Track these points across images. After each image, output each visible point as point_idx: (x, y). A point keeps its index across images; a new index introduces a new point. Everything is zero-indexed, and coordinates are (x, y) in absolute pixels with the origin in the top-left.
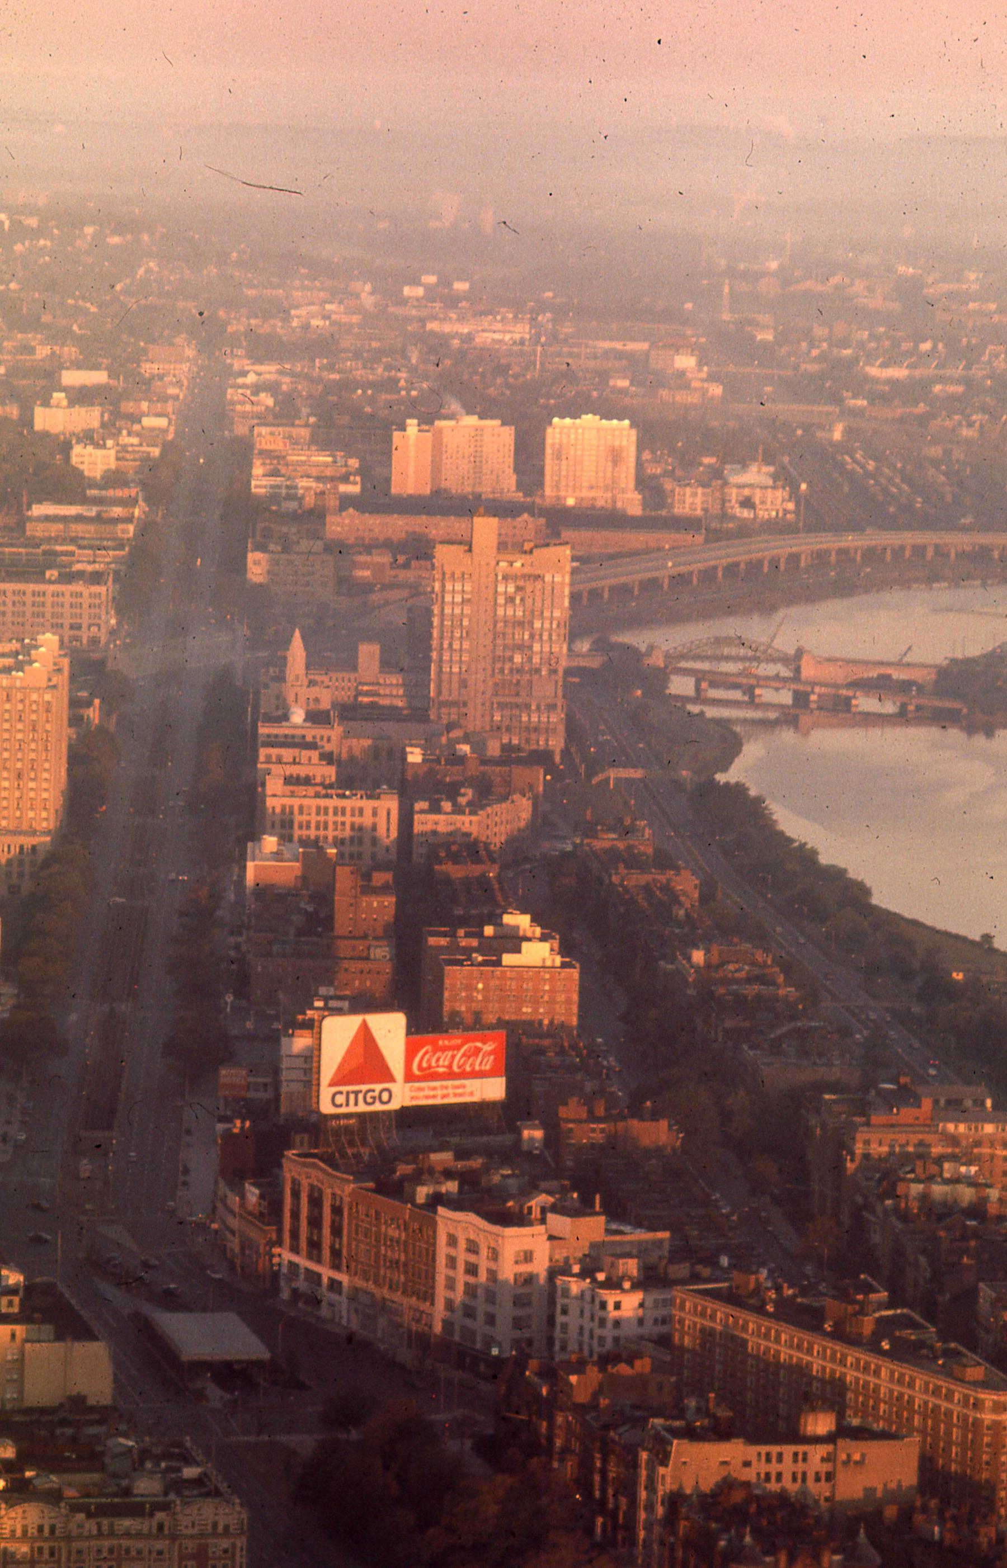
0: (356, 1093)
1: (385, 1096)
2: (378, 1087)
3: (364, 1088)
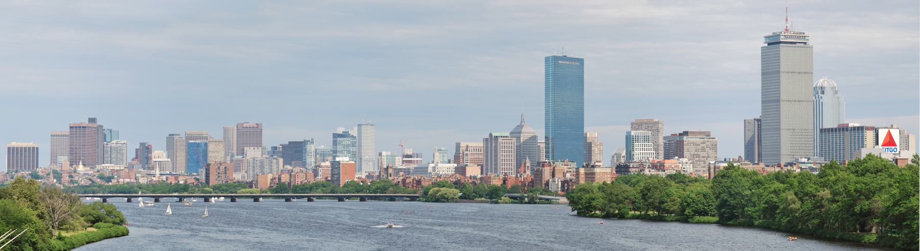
0: (888, 149)
1: (895, 150)
2: (893, 147)
3: (890, 147)
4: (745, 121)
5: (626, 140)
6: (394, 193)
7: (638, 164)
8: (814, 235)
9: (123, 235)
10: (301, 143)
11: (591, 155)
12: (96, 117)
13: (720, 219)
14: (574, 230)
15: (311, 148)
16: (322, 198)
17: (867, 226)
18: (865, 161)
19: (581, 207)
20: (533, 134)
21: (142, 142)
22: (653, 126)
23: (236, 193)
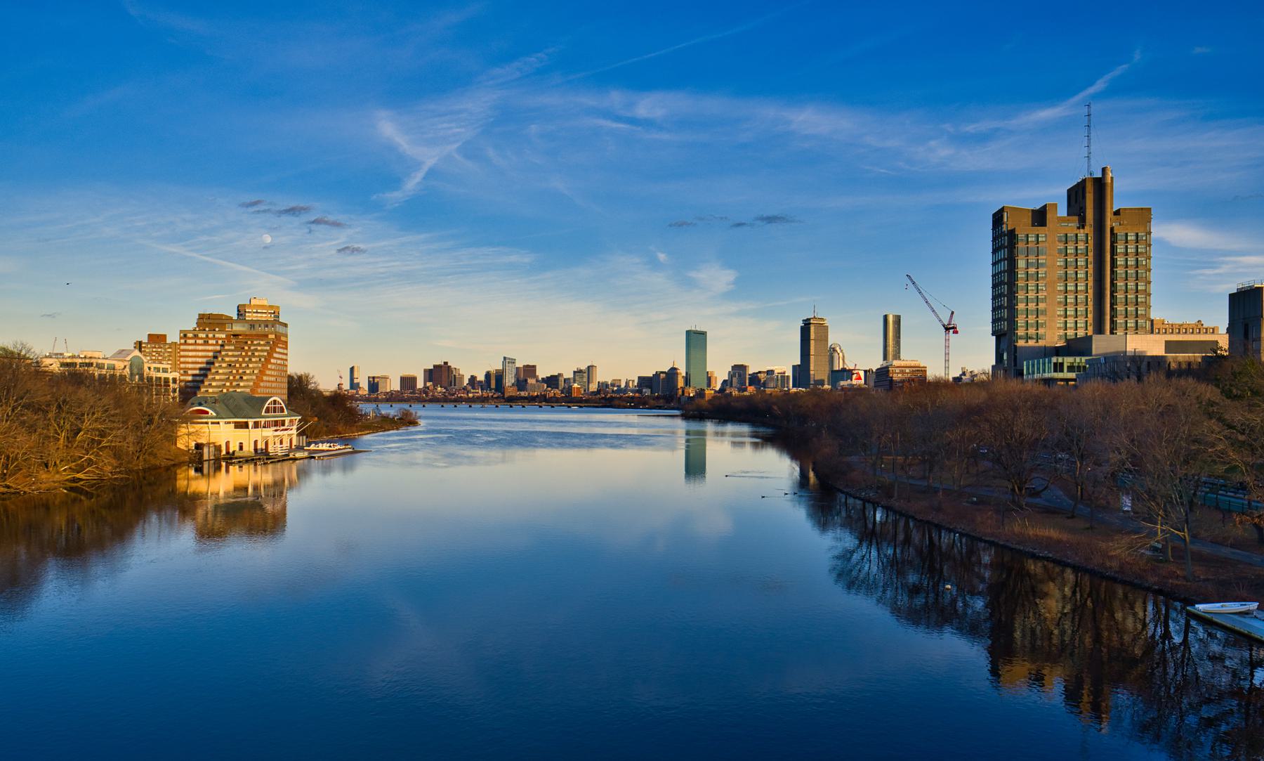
4: (505, 358)
5: (686, 354)
6: (304, 430)
7: (900, 591)
8: (7, 469)
9: (900, 320)
10: (556, 376)
11: (288, 388)
12: (415, 375)
13: (929, 382)
14: (502, 439)
15: (561, 379)
16: (567, 440)
17: (179, 515)
18: (599, 392)
19: (1193, 492)
20: (368, 457)
21: (1103, 335)
22: (513, 361)
23: (235, 422)
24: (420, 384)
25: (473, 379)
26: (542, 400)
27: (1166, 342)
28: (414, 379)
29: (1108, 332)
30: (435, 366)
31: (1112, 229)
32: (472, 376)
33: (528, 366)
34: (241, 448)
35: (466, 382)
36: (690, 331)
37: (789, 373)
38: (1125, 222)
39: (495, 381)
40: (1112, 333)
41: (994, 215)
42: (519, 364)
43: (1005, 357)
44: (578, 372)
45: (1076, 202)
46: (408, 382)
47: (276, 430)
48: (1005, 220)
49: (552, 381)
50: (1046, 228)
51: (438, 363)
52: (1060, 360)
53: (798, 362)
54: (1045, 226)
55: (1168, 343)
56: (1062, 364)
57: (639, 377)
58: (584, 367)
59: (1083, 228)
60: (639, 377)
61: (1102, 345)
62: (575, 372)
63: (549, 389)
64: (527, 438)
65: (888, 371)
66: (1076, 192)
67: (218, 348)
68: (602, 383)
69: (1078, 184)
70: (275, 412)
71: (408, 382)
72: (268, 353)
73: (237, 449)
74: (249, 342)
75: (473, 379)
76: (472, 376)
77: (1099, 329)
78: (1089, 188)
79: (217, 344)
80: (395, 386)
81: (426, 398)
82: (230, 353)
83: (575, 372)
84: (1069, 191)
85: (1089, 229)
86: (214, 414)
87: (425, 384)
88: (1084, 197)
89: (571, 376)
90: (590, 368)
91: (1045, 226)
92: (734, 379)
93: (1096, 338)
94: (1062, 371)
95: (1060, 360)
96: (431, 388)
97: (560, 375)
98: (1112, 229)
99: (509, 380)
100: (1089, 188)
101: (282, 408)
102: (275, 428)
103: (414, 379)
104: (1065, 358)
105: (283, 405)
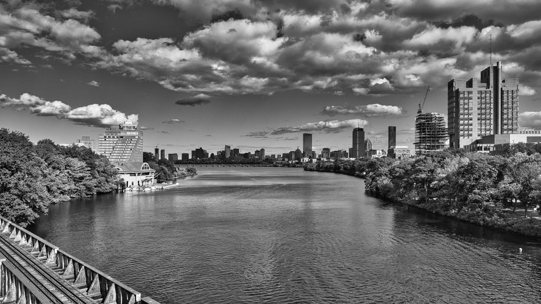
22: (229, 147)
24: (190, 157)
25: (212, 154)
26: (243, 163)
27: (304, 134)
28: (187, 155)
29: (500, 133)
30: (196, 149)
31: (502, 89)
32: (212, 154)
33: (236, 149)
34: (133, 184)
35: (209, 156)
36: (305, 134)
37: (348, 152)
38: (507, 85)
39: (222, 154)
40: (501, 133)
41: (449, 83)
42: (232, 148)
43: (454, 144)
44: (257, 152)
45: (485, 77)
46: (185, 156)
47: (147, 177)
48: (454, 85)
49: (246, 155)
50: (472, 88)
51: (198, 148)
52: (481, 145)
53: (351, 146)
54: (472, 87)
55: (528, 138)
56: (481, 147)
57: (283, 154)
58: (259, 150)
59: (489, 88)
60: (283, 154)
61: (499, 140)
62: (255, 152)
63: (245, 159)
64: (344, 198)
65: (393, 150)
66: (485, 73)
67: (114, 145)
68: (267, 156)
69: (486, 69)
70: (146, 169)
71: (185, 156)
72: (136, 144)
73: (131, 184)
74: (128, 140)
75: (212, 154)
76: (212, 154)
77: (496, 131)
78: (491, 71)
79: (113, 143)
80: (180, 158)
81: (193, 162)
82: (120, 144)
83: (255, 152)
84: (481, 72)
85: (491, 89)
86: (122, 170)
87: (192, 157)
88: (489, 75)
89: (254, 153)
90: (263, 150)
91: (472, 87)
92: (324, 154)
93: (496, 135)
94: (481, 150)
95: (481, 145)
96: (195, 159)
97: (250, 153)
98: (502, 89)
99: (228, 156)
100: (491, 71)
101: (148, 167)
102: (147, 176)
103: (187, 155)
104: (483, 145)
105: (149, 166)
